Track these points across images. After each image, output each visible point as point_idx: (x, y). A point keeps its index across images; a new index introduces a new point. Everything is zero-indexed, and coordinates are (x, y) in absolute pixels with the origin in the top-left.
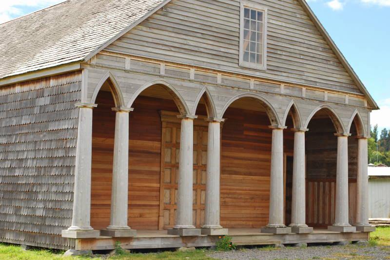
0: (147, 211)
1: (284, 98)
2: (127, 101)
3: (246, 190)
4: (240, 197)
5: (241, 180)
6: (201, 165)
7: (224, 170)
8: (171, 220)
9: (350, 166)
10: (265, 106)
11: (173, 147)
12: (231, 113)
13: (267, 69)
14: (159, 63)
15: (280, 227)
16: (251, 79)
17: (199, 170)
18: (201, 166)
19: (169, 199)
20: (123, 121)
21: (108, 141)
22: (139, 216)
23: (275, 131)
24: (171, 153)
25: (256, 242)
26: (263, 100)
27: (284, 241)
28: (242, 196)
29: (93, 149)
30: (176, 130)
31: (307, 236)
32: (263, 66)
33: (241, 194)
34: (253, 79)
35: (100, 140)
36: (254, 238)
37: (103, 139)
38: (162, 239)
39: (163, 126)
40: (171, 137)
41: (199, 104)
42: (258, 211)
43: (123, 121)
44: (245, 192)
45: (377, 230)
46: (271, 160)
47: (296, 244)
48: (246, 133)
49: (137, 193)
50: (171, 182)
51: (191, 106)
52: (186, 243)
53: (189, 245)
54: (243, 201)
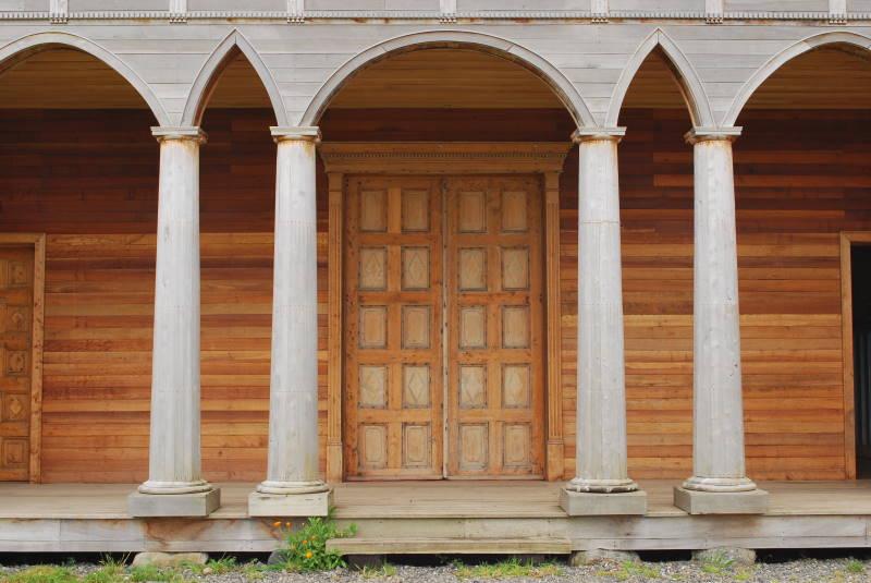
0: (110, 430)
1: (612, 28)
3: (672, 360)
5: (652, 328)
6: (499, 289)
7: (751, 299)
8: (392, 453)
9: (572, 254)
11: (393, 243)
17: (493, 308)
18: (499, 295)
21: (138, 242)
22: (256, 444)
23: (700, 151)
24: (386, 263)
25: (531, 545)
26: (504, 47)
28: (659, 381)
29: (153, 265)
30: (402, 195)
31: (754, 525)
33: (654, 373)
35: (223, 241)
36: (469, 529)
37: (129, 237)
38: (65, 525)
40: (385, 216)
42: (44, 450)
44: (669, 365)
45: (633, 561)
47: (697, 551)
50: (386, 345)
52: (161, 540)
53: (176, 544)
54: (661, 393)
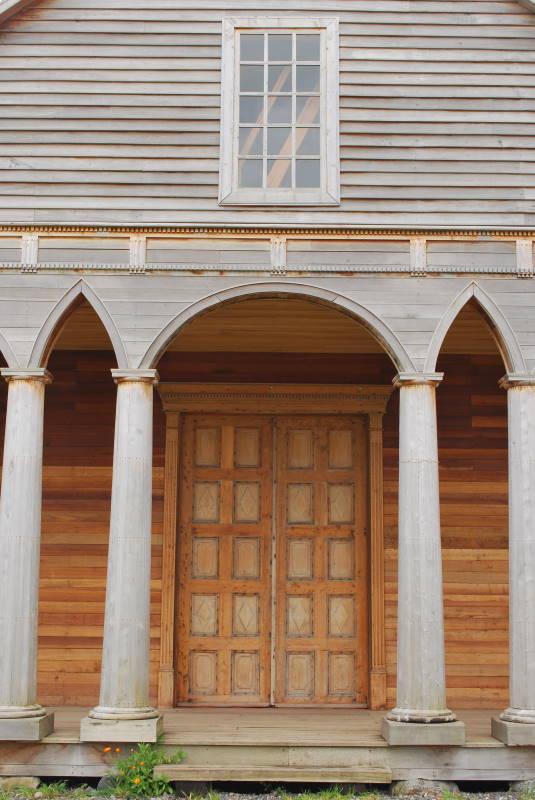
2: (135, 355)
4: (464, 614)
5: (471, 562)
10: (356, 325)
11: (226, 478)
12: (176, 365)
13: (342, 199)
14: (126, 235)
15: (411, 721)
16: (272, 237)
17: (319, 541)
18: (325, 528)
19: (212, 621)
20: (133, 412)
22: (91, 669)
27: (449, 771)
28: (478, 613)
30: (235, 432)
32: (330, 187)
34: (284, 238)
39: (168, 424)
40: (219, 453)
41: (440, 355)
43: (133, 412)
46: (43, 510)
48: (476, 422)
49: (60, 606)
51: (418, 361)
54: (481, 625)
